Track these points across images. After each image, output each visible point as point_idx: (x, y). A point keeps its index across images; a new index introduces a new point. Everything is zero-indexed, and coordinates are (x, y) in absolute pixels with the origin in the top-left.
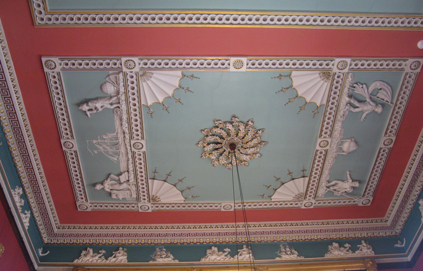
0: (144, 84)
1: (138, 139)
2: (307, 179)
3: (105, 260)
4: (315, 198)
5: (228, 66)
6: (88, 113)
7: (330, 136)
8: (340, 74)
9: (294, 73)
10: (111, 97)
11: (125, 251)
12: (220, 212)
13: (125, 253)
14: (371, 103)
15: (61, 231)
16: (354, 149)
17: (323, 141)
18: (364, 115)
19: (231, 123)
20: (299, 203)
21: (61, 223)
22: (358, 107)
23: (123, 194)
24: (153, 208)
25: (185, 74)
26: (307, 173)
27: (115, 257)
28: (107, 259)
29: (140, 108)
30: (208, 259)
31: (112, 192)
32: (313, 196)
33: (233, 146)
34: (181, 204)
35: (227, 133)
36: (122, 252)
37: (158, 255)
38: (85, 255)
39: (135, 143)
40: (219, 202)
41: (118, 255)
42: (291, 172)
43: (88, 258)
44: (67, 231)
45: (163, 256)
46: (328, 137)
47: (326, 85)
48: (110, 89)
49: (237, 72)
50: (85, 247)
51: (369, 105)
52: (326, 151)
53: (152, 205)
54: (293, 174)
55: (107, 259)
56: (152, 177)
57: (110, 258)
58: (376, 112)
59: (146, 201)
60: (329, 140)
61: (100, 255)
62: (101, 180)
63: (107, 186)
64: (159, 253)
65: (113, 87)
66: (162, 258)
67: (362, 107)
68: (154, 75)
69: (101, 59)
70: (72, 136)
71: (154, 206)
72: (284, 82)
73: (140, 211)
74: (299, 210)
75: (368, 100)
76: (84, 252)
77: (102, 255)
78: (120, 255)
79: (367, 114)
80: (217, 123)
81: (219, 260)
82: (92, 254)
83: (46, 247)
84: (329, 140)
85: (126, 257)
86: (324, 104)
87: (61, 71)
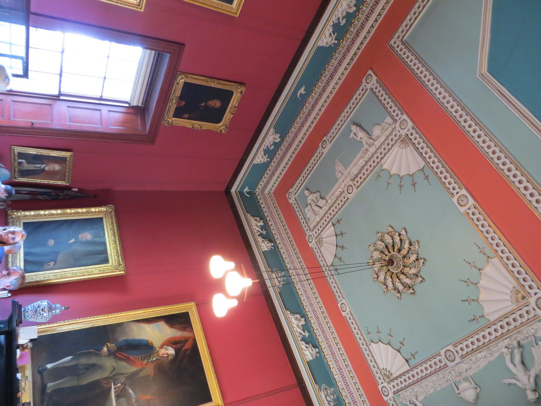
0: (397, 148)
1: (355, 185)
2: (407, 367)
3: (299, 339)
4: (395, 393)
5: (533, 294)
6: (352, 135)
7: (463, 357)
8: (532, 311)
9: (496, 261)
10: (371, 139)
11: (316, 356)
12: (336, 303)
13: (314, 356)
14: (532, 380)
15: (268, 197)
16: (471, 401)
17: (453, 353)
18: (513, 381)
19: (411, 244)
20: (382, 381)
21: (274, 193)
22: (515, 365)
23: (311, 216)
24: (347, 315)
25: (425, 169)
26: (413, 362)
27: (306, 347)
28: (302, 340)
29: (378, 163)
30: (290, 316)
31: (309, 206)
32: (395, 390)
33: (391, 262)
34: (378, 368)
35: (406, 255)
36: (314, 353)
37: (327, 392)
38: (297, 318)
39: (451, 351)
40: (344, 296)
41: (310, 349)
42: (344, 235)
43: (254, 222)
44: (269, 200)
45: (328, 398)
46: (460, 355)
47: (510, 306)
48: (376, 131)
49: (456, 206)
50: (262, 218)
51: (527, 377)
52: (446, 366)
53: (349, 313)
54: (403, 347)
55: (302, 340)
56: (334, 223)
57: (260, 237)
58: (526, 395)
59: (393, 390)
60: (458, 360)
61: (260, 230)
62: (313, 191)
63: (311, 198)
64: (329, 392)
65: (379, 132)
66: (326, 397)
67: (518, 371)
68: (408, 149)
69: (431, 149)
70: (358, 187)
71: (349, 315)
72: (419, 179)
73: (339, 305)
74: (375, 384)
75: (533, 373)
76: (298, 316)
77: (303, 334)
78: (311, 351)
79: (515, 384)
80: (403, 232)
81: (293, 327)
82: (300, 324)
83: (252, 193)
84: (458, 360)
85: (311, 358)
86: (490, 321)
87: (369, 90)
